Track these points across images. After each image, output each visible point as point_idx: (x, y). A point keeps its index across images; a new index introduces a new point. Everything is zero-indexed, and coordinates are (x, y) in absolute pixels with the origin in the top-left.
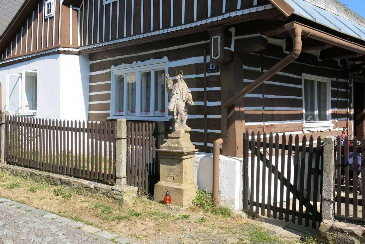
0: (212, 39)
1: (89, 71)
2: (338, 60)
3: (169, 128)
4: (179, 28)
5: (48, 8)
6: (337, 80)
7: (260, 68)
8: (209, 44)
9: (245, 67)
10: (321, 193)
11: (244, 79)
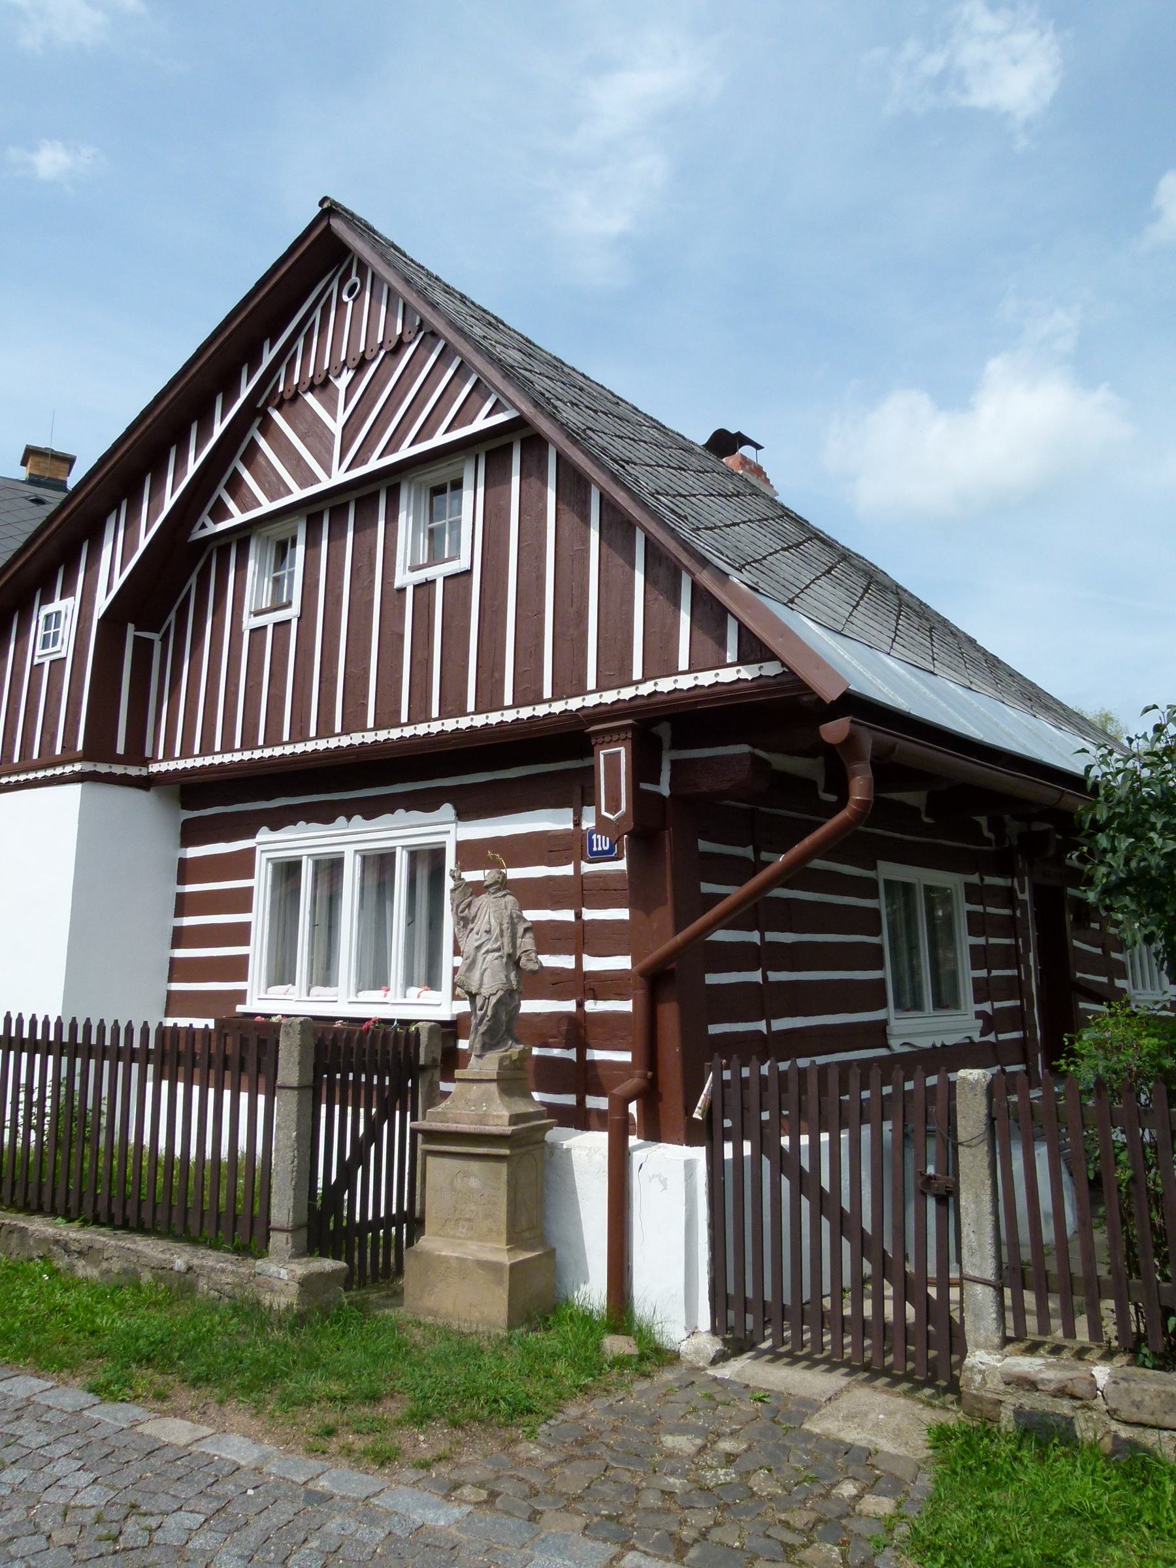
0: (602, 757)
1: (179, 841)
2: (983, 820)
3: (456, 1043)
4: (494, 718)
5: (47, 627)
6: (982, 880)
7: (751, 847)
8: (592, 771)
9: (704, 845)
10: (959, 1260)
11: (702, 884)
